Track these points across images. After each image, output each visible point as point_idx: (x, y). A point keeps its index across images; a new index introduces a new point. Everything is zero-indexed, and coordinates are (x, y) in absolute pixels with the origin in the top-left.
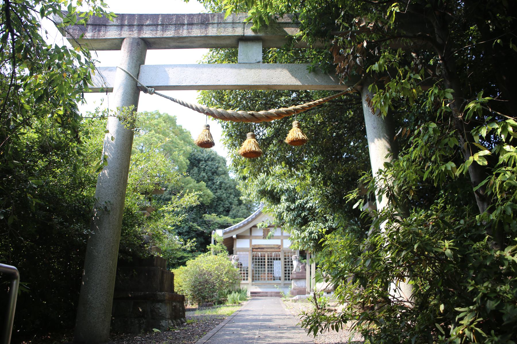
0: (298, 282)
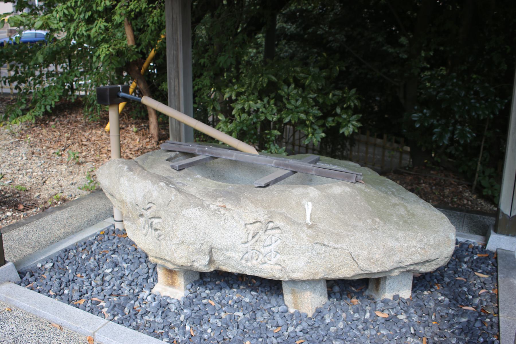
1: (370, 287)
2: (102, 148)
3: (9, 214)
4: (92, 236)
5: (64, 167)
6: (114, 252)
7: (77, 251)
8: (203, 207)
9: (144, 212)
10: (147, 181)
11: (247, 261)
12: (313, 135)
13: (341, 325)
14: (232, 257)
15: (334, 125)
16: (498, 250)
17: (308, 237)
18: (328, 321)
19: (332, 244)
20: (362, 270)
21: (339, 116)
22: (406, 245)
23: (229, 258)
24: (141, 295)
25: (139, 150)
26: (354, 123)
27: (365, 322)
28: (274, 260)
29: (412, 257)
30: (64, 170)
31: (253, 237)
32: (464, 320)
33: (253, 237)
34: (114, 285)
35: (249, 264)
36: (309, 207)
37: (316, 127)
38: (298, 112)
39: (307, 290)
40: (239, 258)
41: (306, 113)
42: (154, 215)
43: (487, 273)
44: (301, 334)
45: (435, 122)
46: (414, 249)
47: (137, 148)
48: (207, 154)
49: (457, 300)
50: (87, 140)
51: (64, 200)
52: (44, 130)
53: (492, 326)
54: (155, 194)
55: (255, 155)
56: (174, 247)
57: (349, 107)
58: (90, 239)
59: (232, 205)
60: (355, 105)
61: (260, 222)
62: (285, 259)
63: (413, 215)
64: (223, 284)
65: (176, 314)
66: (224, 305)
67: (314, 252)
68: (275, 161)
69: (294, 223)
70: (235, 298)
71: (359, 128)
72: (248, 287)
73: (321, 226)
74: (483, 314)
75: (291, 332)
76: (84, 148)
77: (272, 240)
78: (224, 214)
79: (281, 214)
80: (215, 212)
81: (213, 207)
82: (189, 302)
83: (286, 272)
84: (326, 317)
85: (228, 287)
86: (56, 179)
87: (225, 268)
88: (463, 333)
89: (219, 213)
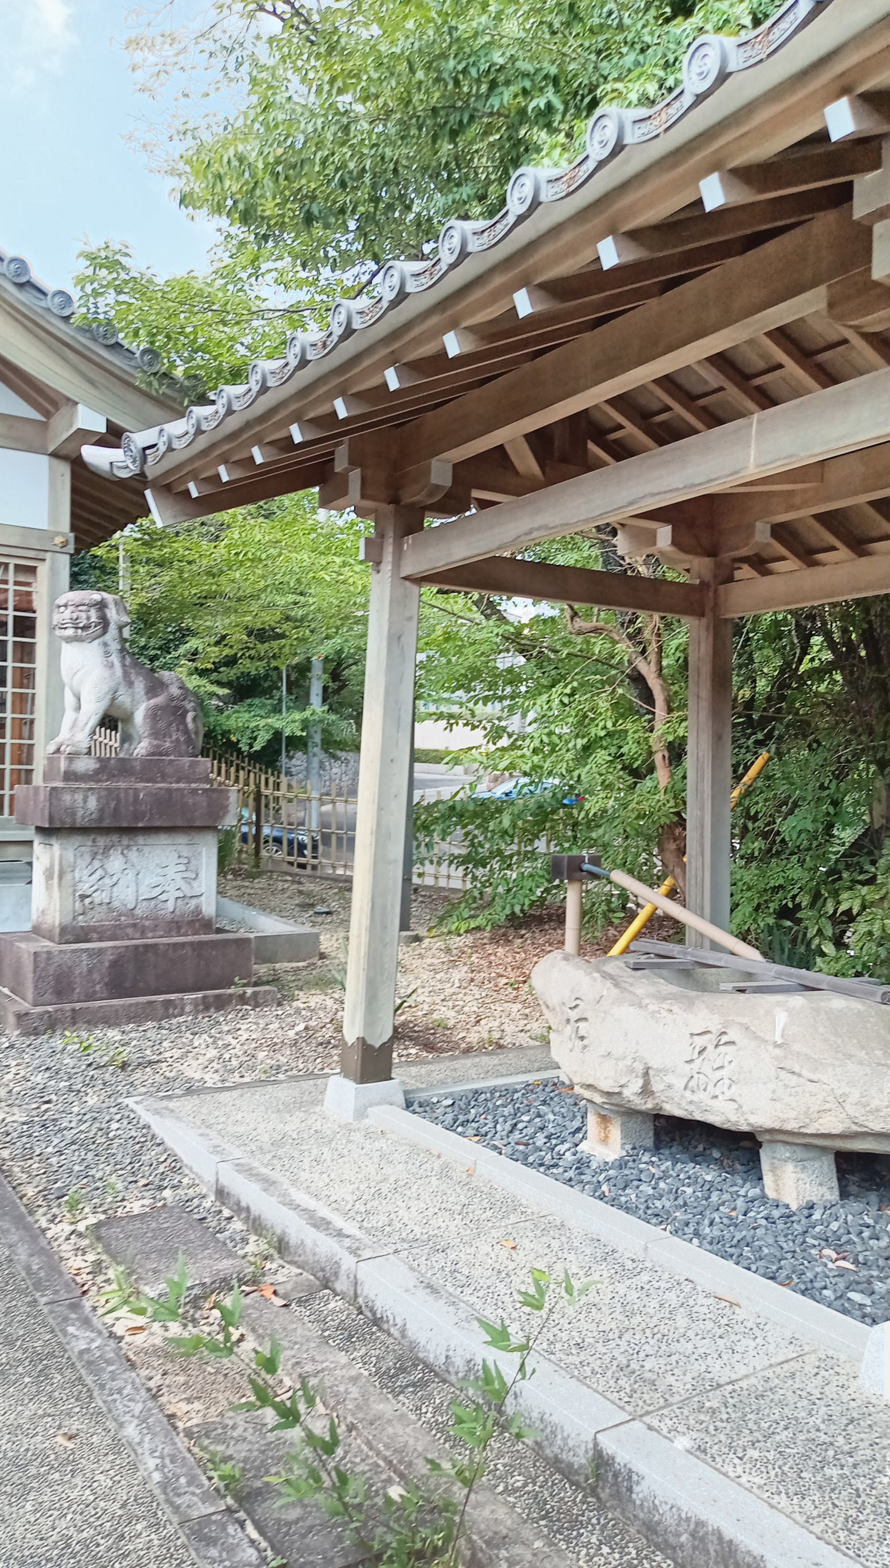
0: (115, 862)
3: (413, 1051)
8: (641, 1007)
19: (805, 1073)
36: (781, 1017)
51: (501, 1047)
52: (500, 950)
73: (796, 1047)
81: (651, 1007)
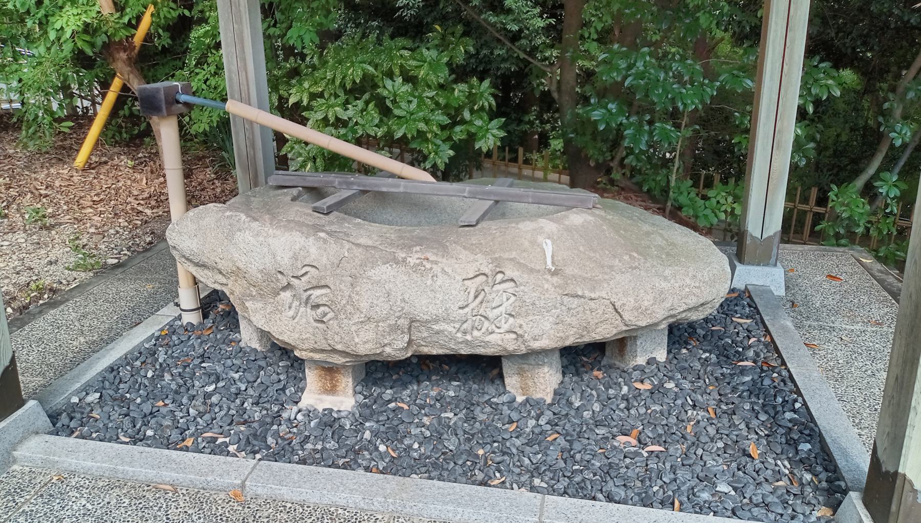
1: (607, 353)
2: (81, 198)
4: (148, 340)
5: (20, 237)
6: (203, 357)
7: (132, 368)
9: (295, 282)
10: (294, 233)
11: (465, 333)
12: (436, 154)
13: (597, 407)
14: (443, 331)
15: (463, 137)
16: (749, 287)
17: (555, 287)
18: (577, 404)
19: (587, 294)
20: (627, 325)
21: (470, 123)
22: (677, 285)
23: (438, 333)
24: (285, 415)
25: (150, 196)
26: (495, 132)
27: (625, 398)
28: (505, 327)
29: (686, 301)
30: (23, 240)
31: (476, 297)
32: (747, 379)
33: (476, 297)
34: (229, 409)
35: (469, 337)
37: (439, 142)
38: (415, 120)
39: (544, 364)
40: (454, 331)
41: (427, 122)
42: (315, 283)
43: (747, 318)
44: (548, 427)
45: (625, 121)
46: (687, 290)
47: (146, 195)
48: (355, 187)
49: (727, 355)
50: (47, 188)
53: (783, 381)
54: (313, 250)
55: (433, 183)
56: (354, 328)
57: (482, 108)
58: (147, 346)
59: (437, 255)
60: (490, 105)
61: (484, 274)
62: (522, 322)
63: (673, 244)
64: (406, 378)
65: (355, 431)
66: (422, 407)
67: (564, 308)
68: (468, 189)
69: (532, 271)
70: (433, 393)
71: (502, 139)
72: (443, 377)
74: (765, 368)
75: (534, 427)
76: (44, 200)
77: (501, 299)
78: (431, 269)
79: (511, 260)
80: (415, 268)
82: (365, 412)
83: (524, 342)
84: (573, 399)
85: (414, 381)
86: (14, 257)
87: (426, 350)
88: (752, 396)
89: (423, 268)
